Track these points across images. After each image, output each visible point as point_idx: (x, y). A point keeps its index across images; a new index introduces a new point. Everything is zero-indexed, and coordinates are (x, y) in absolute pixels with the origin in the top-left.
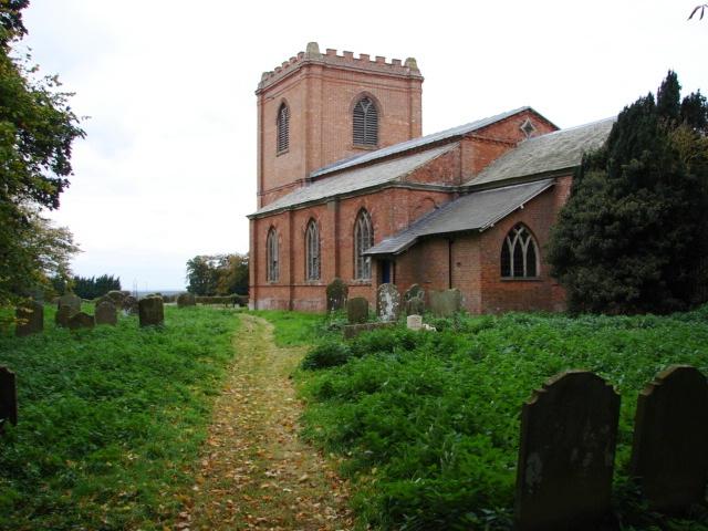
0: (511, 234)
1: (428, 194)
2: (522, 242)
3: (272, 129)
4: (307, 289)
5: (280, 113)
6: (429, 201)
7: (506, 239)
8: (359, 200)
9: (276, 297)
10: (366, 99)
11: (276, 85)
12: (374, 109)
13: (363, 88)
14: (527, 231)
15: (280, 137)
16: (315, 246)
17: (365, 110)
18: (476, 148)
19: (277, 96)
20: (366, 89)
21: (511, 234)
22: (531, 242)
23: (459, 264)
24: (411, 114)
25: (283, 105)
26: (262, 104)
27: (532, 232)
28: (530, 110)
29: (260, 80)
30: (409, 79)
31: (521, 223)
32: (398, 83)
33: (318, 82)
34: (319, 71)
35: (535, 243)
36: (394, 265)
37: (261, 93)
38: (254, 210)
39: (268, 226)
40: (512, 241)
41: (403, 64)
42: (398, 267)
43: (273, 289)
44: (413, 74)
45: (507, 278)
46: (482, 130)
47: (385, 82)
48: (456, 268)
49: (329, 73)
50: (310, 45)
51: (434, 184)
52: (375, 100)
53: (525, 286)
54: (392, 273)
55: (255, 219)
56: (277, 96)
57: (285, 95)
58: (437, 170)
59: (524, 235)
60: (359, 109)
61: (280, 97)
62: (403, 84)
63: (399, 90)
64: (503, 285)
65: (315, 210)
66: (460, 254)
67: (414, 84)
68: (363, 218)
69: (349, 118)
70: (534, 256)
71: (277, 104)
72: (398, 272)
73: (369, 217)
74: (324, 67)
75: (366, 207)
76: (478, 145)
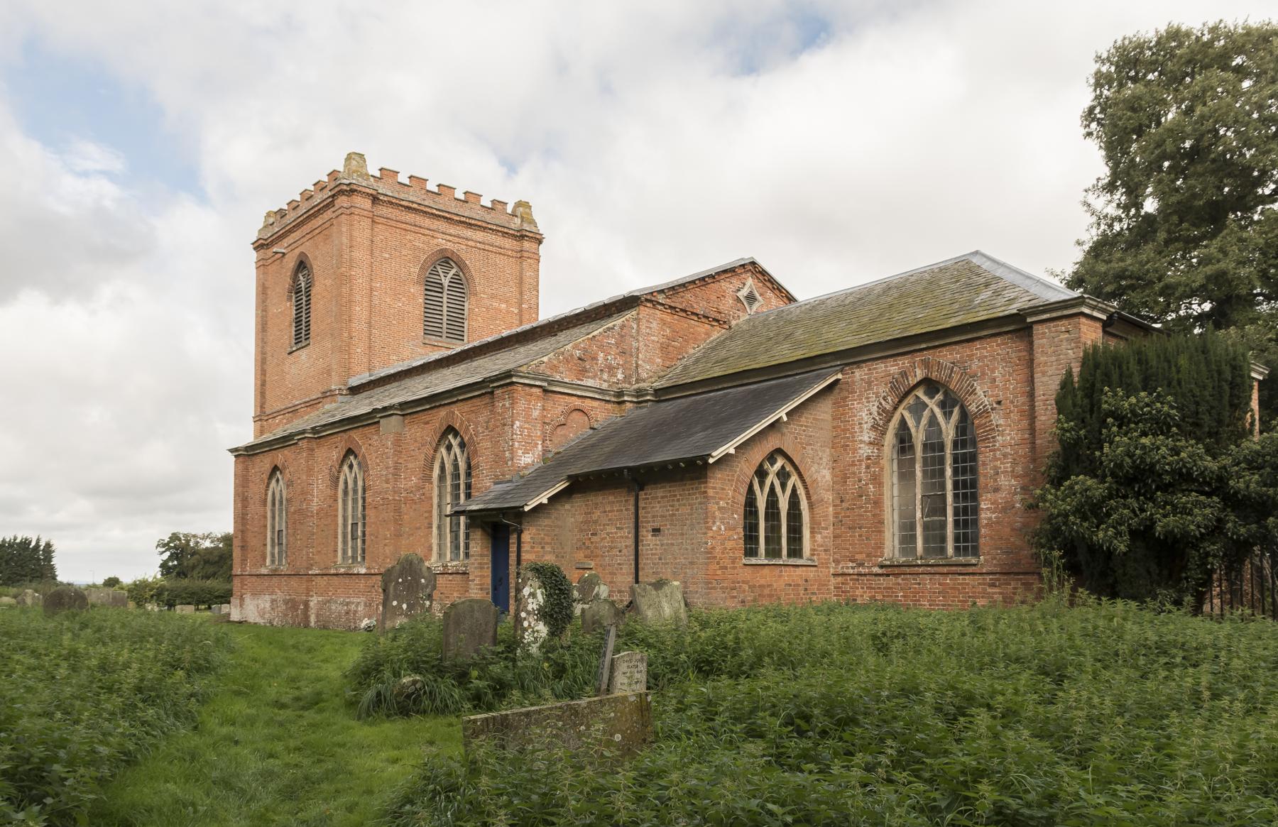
0: (761, 473)
1: (578, 402)
2: (911, 423)
3: (285, 309)
4: (335, 580)
5: (295, 278)
6: (576, 415)
7: (751, 486)
8: (443, 412)
9: (279, 596)
10: (446, 259)
11: (290, 231)
12: (461, 284)
13: (441, 242)
14: (789, 468)
15: (298, 321)
16: (355, 501)
17: (446, 282)
18: (663, 322)
19: (290, 250)
20: (449, 246)
21: (761, 473)
22: (794, 490)
23: (656, 531)
24: (521, 293)
25: (302, 265)
26: (262, 265)
27: (796, 468)
28: (753, 263)
29: (261, 225)
30: (521, 236)
31: (779, 451)
32: (498, 240)
33: (366, 223)
34: (367, 203)
35: (801, 492)
36: (520, 533)
37: (260, 246)
38: (247, 436)
39: (267, 467)
40: (762, 484)
41: (509, 210)
42: (526, 537)
43: (275, 580)
44: (526, 226)
45: (753, 561)
46: (675, 289)
47: (479, 235)
48: (648, 538)
49: (384, 211)
50: (349, 157)
51: (590, 383)
52: (461, 266)
53: (786, 572)
54: (513, 548)
55: (245, 455)
56: (290, 250)
57: (307, 248)
58: (595, 359)
59: (783, 475)
60: (434, 278)
61: (297, 252)
62: (509, 243)
63: (501, 251)
64: (747, 574)
65: (356, 435)
66: (658, 508)
67: (527, 245)
68: (449, 448)
69: (417, 291)
70: (800, 515)
71: (291, 262)
72: (525, 547)
73: (462, 445)
74: (375, 199)
75: (457, 426)
76: (668, 318)
